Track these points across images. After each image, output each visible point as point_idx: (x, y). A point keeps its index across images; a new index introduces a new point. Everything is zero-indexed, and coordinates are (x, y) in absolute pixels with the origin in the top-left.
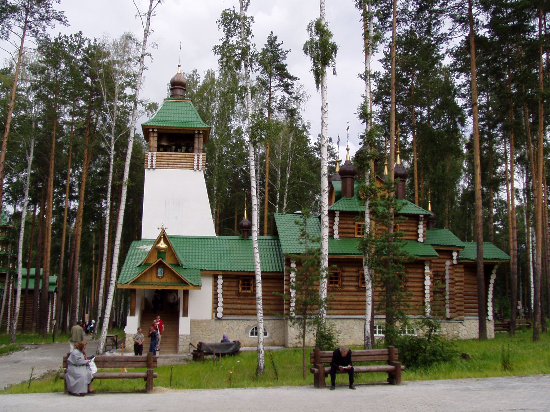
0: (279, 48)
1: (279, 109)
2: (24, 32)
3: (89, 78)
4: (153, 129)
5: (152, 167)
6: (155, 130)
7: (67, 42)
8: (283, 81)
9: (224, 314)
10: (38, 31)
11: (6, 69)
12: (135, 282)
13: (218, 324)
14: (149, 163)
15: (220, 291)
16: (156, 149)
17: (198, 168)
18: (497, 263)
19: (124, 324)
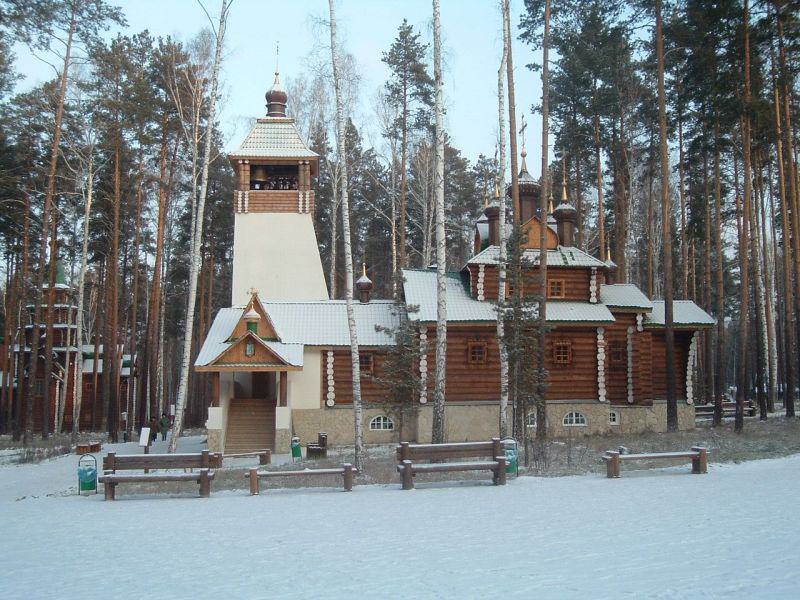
0: (416, 42)
1: (418, 126)
2: (71, 36)
3: (161, 90)
4: (244, 160)
5: (243, 211)
6: (247, 162)
7: (129, 45)
8: (421, 88)
9: (336, 402)
10: (89, 34)
11: (53, 82)
12: (217, 362)
13: (328, 412)
14: (240, 205)
15: (330, 371)
16: (249, 187)
17: (304, 211)
18: (697, 329)
19: (206, 416)
